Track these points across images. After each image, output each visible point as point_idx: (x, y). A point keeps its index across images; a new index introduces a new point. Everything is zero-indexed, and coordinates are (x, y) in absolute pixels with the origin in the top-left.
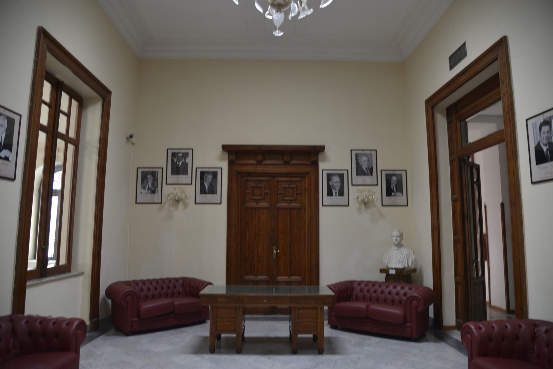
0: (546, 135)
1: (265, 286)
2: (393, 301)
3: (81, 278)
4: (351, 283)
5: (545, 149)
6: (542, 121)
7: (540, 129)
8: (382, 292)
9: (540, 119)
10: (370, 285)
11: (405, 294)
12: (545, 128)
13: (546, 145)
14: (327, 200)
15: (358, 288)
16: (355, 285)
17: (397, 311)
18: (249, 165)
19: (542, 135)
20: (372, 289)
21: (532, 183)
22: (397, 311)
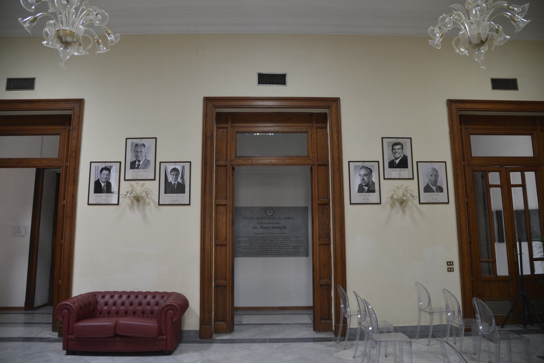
0: (105, 176)
1: (516, 336)
2: (143, 313)
3: (168, 167)
4: (94, 295)
5: (103, 185)
6: (104, 167)
7: (101, 171)
8: (140, 304)
9: (103, 165)
10: (116, 296)
11: (157, 304)
12: (105, 172)
13: (104, 182)
14: (358, 197)
15: (102, 301)
16: (99, 298)
17: (151, 324)
18: (454, 106)
19: (102, 176)
20: (136, 302)
21: (88, 204)
22: (151, 324)
